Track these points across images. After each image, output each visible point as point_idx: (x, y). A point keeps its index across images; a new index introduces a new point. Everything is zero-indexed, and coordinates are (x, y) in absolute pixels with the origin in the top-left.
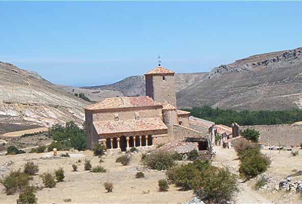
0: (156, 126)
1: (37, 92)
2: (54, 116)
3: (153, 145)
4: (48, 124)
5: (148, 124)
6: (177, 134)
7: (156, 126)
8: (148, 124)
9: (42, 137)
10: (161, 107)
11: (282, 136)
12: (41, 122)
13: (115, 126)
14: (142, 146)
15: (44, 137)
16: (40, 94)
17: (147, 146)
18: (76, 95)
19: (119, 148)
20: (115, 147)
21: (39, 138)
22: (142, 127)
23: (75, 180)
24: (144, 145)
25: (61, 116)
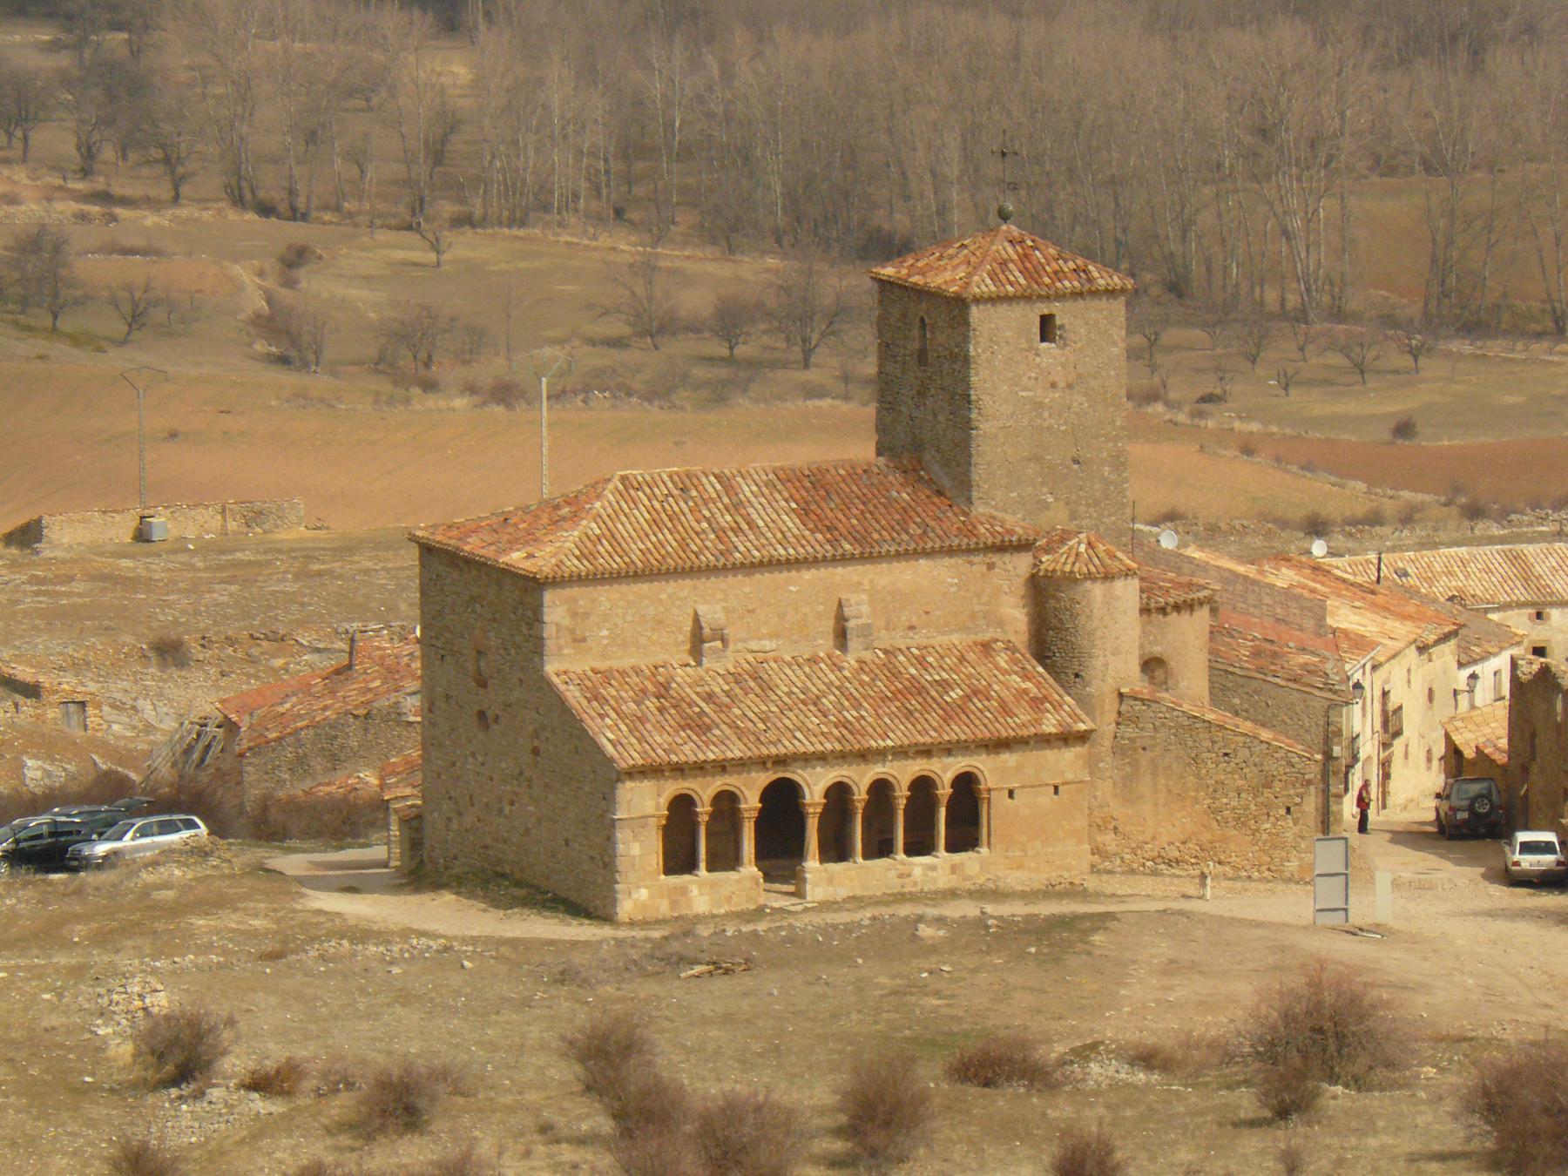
3: (984, 850)
5: (945, 685)
6: (1144, 759)
8: (945, 685)
14: (911, 850)
20: (725, 859)
24: (920, 845)
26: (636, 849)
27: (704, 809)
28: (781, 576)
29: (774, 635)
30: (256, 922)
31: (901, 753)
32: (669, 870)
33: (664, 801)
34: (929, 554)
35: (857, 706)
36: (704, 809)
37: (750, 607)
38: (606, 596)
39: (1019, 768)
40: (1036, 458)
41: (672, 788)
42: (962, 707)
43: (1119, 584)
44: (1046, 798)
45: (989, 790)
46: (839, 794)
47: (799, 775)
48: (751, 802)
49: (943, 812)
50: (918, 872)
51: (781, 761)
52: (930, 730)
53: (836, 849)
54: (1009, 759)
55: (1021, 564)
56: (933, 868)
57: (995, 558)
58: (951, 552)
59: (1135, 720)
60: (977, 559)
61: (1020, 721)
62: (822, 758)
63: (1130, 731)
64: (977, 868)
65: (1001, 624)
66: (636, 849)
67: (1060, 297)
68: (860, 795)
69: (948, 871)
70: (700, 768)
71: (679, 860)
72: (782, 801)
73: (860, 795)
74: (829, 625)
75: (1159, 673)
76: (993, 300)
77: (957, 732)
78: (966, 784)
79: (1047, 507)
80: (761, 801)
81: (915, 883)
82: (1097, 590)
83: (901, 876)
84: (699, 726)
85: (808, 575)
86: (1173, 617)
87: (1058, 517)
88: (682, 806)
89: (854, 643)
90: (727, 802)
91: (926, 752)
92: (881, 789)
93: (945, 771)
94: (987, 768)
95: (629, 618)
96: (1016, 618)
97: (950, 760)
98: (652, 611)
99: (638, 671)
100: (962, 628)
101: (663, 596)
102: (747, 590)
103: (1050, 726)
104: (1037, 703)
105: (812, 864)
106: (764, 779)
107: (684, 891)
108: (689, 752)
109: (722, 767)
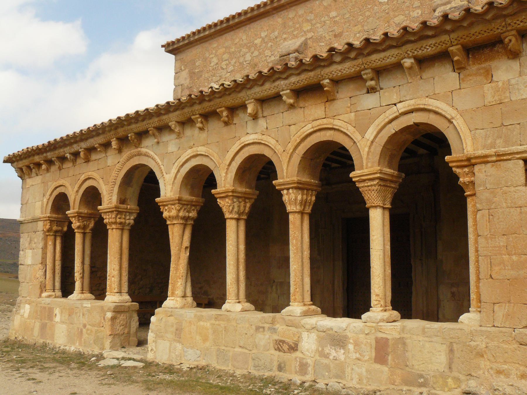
19: (116, 296)
26: (29, 253)
37: (338, 30)
45: (470, 163)
46: (201, 180)
50: (309, 343)
56: (339, 341)
64: (440, 360)
69: (369, 353)
80: (138, 205)
81: (303, 368)
83: (279, 345)
92: (259, 171)
93: (366, 125)
94: (458, 106)
95: (231, 68)
97: (370, 101)
98: (248, 57)
101: (258, 41)
102: (333, 14)
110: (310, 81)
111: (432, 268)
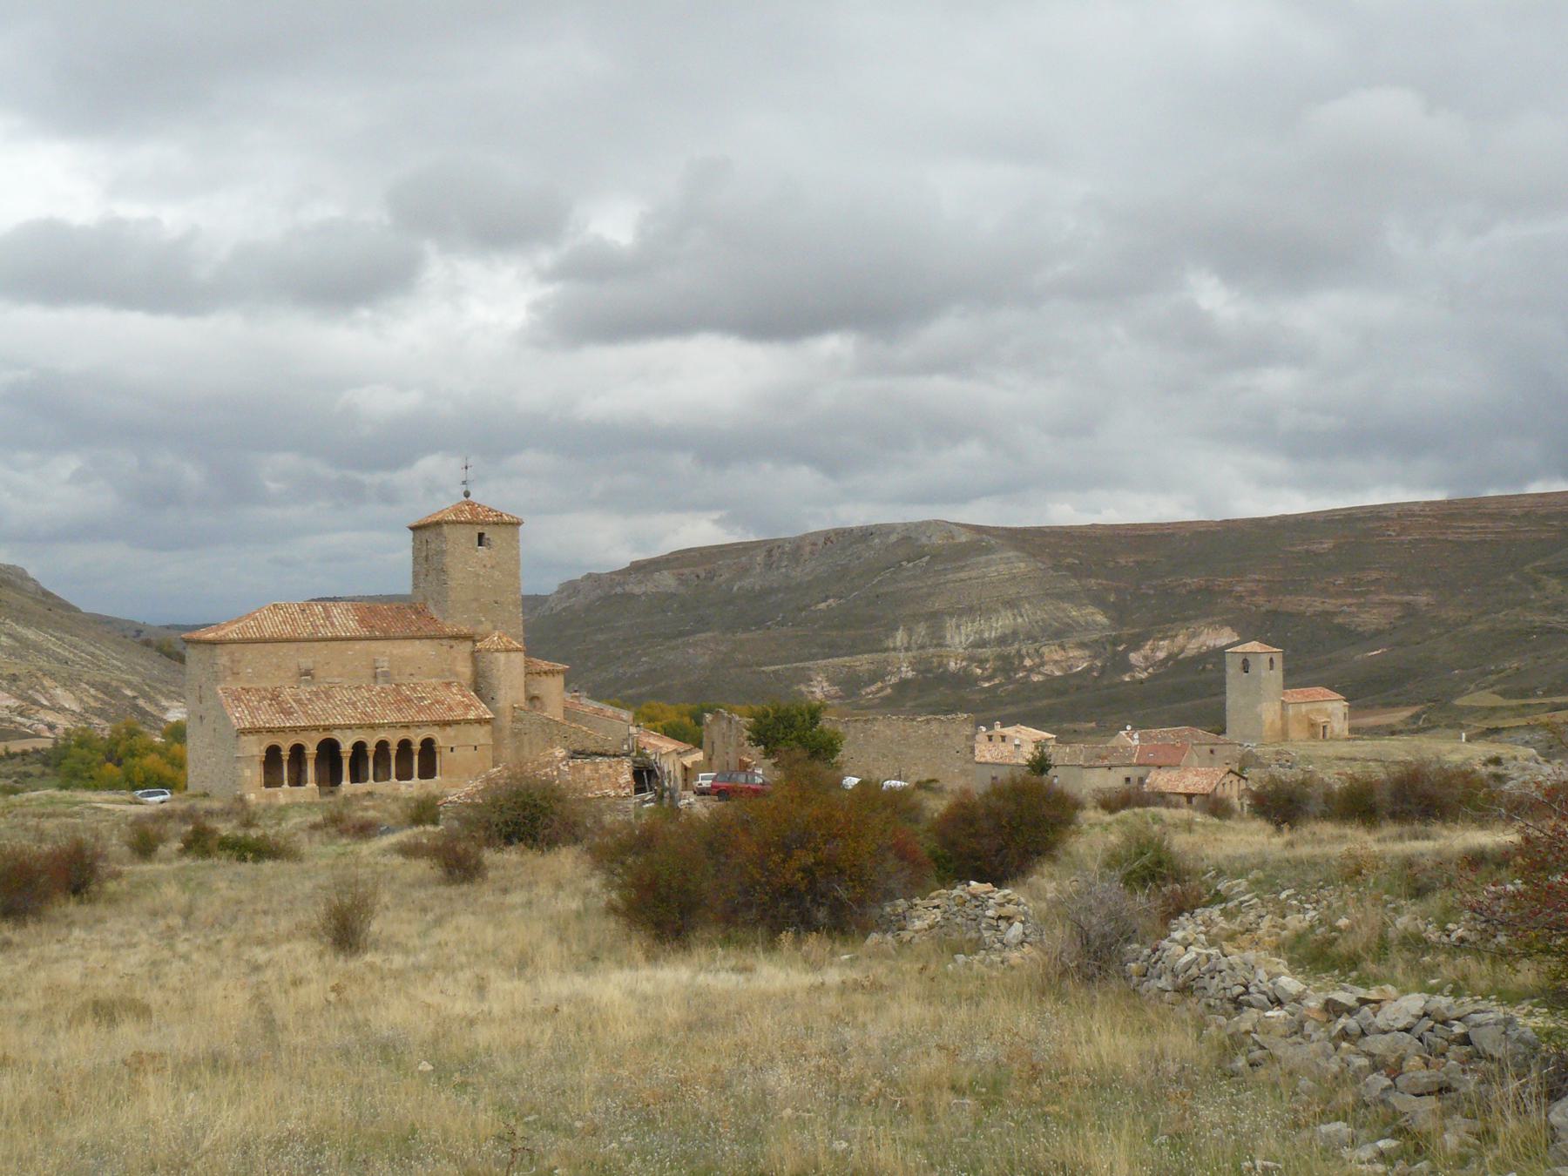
0: (450, 709)
1: (19, 629)
2: (75, 707)
3: (438, 778)
4: (51, 727)
5: (422, 698)
6: (526, 738)
7: (450, 709)
8: (422, 698)
9: (30, 769)
10: (470, 638)
11: (885, 756)
12: (28, 722)
13: (299, 701)
14: (399, 778)
15: (36, 769)
16: (30, 634)
17: (416, 780)
18: (147, 643)
19: (311, 784)
20: (298, 780)
21: (23, 769)
22: (400, 710)
23: (280, 764)
24: (404, 775)
25: (98, 705)
26: (248, 773)
27: (416, 747)
28: (344, 645)
29: (340, 676)
30: (1039, 704)
31: (392, 726)
32: (267, 785)
33: (263, 748)
34: (419, 638)
35: (374, 705)
36: (416, 747)
38: (250, 652)
39: (456, 737)
40: (476, 600)
41: (269, 740)
42: (429, 707)
43: (513, 655)
44: (470, 752)
46: (359, 748)
47: (336, 735)
48: (311, 750)
49: (416, 758)
51: (326, 728)
52: (410, 715)
53: (356, 777)
54: (450, 731)
55: (467, 647)
57: (453, 642)
58: (431, 638)
59: (520, 720)
60: (444, 642)
61: (458, 714)
62: (349, 727)
63: (519, 726)
65: (456, 675)
66: (248, 773)
67: (488, 524)
68: (371, 748)
70: (282, 730)
71: (271, 779)
72: (329, 750)
73: (371, 748)
74: (370, 672)
75: (538, 704)
76: (453, 523)
77: (423, 717)
78: (428, 744)
79: (481, 622)
82: (502, 657)
84: (288, 713)
85: (358, 646)
86: (544, 677)
87: (488, 626)
88: (273, 753)
89: (380, 679)
90: (298, 750)
91: (406, 726)
94: (440, 738)
96: (465, 669)
99: (265, 690)
100: (436, 676)
103: (472, 715)
104: (467, 707)
105: (346, 782)
106: (319, 737)
107: (276, 795)
108: (278, 721)
109: (294, 729)
110: (406, 726)
111: (428, 771)
